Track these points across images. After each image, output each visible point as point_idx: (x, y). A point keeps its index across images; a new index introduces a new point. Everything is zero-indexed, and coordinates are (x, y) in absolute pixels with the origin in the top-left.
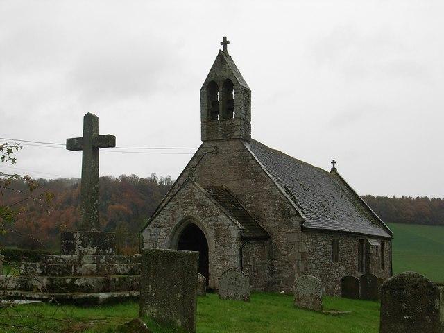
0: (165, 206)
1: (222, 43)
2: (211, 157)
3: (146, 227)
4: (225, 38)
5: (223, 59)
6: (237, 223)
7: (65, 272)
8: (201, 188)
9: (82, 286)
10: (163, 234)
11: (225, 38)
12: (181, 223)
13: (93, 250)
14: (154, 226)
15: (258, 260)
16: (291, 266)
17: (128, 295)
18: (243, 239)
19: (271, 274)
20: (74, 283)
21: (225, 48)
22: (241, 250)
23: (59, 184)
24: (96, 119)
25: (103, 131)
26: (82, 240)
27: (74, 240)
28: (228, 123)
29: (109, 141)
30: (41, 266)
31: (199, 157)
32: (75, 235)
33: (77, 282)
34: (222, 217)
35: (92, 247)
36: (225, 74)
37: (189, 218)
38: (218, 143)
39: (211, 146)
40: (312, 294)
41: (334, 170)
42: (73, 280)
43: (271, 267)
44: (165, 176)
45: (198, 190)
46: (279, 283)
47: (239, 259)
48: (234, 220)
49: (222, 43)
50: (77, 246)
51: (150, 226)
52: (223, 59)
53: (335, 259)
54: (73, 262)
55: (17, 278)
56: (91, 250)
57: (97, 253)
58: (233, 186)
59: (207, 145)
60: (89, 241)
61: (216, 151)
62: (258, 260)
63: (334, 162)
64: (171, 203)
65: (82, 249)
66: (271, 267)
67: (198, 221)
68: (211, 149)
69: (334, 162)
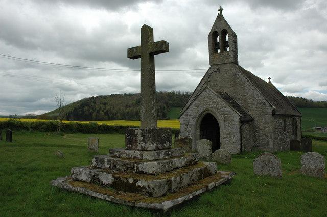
0: (191, 105)
1: (219, 10)
4: (221, 7)
5: (220, 17)
7: (129, 168)
8: (214, 92)
10: (192, 120)
11: (221, 7)
12: (202, 113)
17: (191, 197)
18: (242, 122)
19: (255, 141)
21: (221, 12)
22: (240, 128)
23: (130, 95)
25: (157, 38)
26: (143, 136)
27: (136, 136)
28: (225, 54)
29: (163, 47)
30: (108, 160)
31: (208, 76)
32: (136, 131)
33: (139, 184)
36: (223, 26)
38: (220, 66)
39: (216, 68)
41: (270, 82)
42: (136, 181)
45: (211, 93)
46: (259, 146)
47: (239, 134)
49: (219, 10)
50: (139, 142)
51: (184, 116)
52: (220, 17)
53: (285, 130)
54: (135, 158)
56: (151, 145)
57: (157, 149)
58: (229, 91)
59: (213, 67)
61: (219, 70)
63: (270, 79)
65: (143, 144)
66: (254, 137)
68: (216, 70)
69: (270, 79)
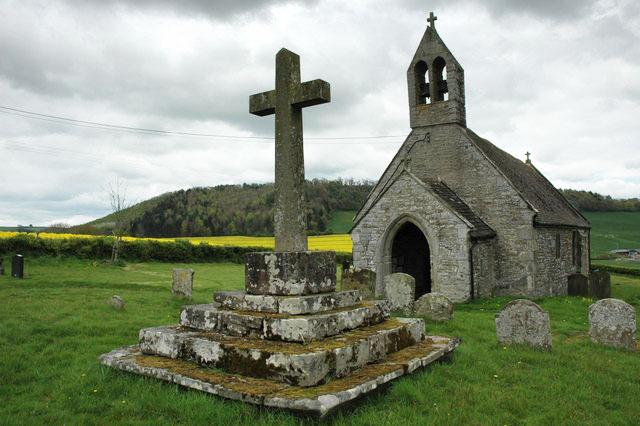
2: (422, 146)
3: (355, 226)
5: (431, 34)
6: (465, 220)
7: (253, 330)
8: (420, 181)
9: (281, 369)
12: (395, 222)
13: (299, 287)
14: (365, 226)
15: (485, 262)
16: (523, 268)
17: (374, 386)
18: (473, 239)
19: (498, 277)
20: (268, 362)
21: (433, 24)
22: (470, 252)
24: (295, 59)
25: (307, 75)
26: (281, 268)
27: (266, 267)
28: (441, 105)
29: (319, 93)
31: (407, 148)
32: (267, 258)
33: (271, 361)
34: (446, 213)
35: (298, 281)
36: (436, 52)
37: (407, 215)
38: (430, 130)
39: (422, 134)
40: (618, 326)
41: (528, 161)
42: (266, 355)
43: (498, 268)
44: (349, 178)
46: (507, 287)
48: (461, 217)
49: (428, 20)
50: (271, 278)
51: (359, 227)
52: (431, 34)
53: (558, 256)
55: (172, 337)
56: (296, 285)
57: (308, 292)
60: (293, 271)
62: (485, 262)
64: (383, 199)
65: (280, 283)
66: (498, 268)
67: (418, 221)
69: (528, 154)
